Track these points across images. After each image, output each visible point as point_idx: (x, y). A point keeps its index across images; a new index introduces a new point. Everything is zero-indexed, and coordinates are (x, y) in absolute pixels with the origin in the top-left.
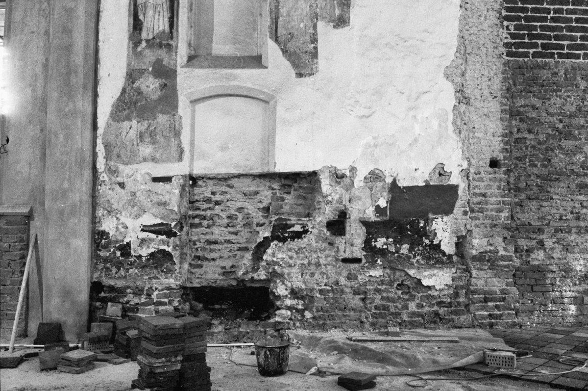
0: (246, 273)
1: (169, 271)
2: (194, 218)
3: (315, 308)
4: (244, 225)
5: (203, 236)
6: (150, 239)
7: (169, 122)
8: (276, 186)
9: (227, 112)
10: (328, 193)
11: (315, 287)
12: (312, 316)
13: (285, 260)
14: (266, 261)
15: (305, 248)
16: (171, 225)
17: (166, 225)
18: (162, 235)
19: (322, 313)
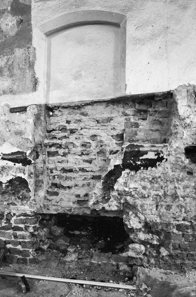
0: (97, 203)
1: (24, 198)
2: (51, 146)
3: (171, 245)
4: (98, 153)
5: (59, 165)
6: (8, 167)
7: (24, 54)
8: (130, 111)
9: (80, 42)
10: (186, 116)
11: (172, 222)
12: (169, 254)
13: (138, 190)
14: (118, 190)
15: (160, 177)
16: (26, 153)
17: (22, 153)
18: (19, 163)
19: (179, 252)
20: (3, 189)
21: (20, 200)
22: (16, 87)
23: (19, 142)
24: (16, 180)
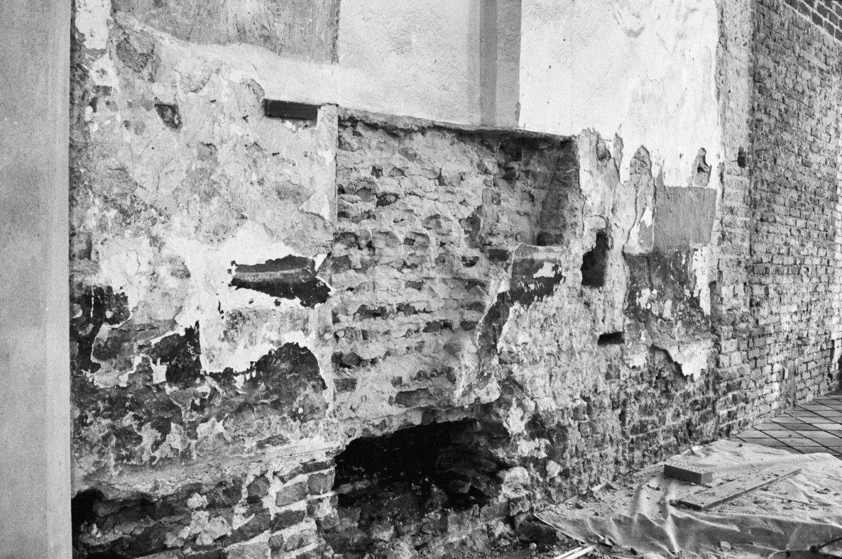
16: (313, 262)
18: (291, 297)
20: (237, 394)
21: (298, 421)
22: (282, 26)
23: (290, 225)
24: (280, 358)
